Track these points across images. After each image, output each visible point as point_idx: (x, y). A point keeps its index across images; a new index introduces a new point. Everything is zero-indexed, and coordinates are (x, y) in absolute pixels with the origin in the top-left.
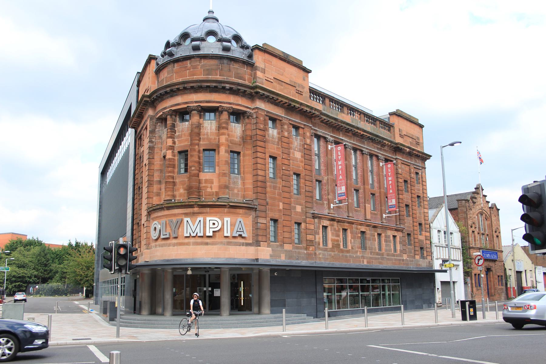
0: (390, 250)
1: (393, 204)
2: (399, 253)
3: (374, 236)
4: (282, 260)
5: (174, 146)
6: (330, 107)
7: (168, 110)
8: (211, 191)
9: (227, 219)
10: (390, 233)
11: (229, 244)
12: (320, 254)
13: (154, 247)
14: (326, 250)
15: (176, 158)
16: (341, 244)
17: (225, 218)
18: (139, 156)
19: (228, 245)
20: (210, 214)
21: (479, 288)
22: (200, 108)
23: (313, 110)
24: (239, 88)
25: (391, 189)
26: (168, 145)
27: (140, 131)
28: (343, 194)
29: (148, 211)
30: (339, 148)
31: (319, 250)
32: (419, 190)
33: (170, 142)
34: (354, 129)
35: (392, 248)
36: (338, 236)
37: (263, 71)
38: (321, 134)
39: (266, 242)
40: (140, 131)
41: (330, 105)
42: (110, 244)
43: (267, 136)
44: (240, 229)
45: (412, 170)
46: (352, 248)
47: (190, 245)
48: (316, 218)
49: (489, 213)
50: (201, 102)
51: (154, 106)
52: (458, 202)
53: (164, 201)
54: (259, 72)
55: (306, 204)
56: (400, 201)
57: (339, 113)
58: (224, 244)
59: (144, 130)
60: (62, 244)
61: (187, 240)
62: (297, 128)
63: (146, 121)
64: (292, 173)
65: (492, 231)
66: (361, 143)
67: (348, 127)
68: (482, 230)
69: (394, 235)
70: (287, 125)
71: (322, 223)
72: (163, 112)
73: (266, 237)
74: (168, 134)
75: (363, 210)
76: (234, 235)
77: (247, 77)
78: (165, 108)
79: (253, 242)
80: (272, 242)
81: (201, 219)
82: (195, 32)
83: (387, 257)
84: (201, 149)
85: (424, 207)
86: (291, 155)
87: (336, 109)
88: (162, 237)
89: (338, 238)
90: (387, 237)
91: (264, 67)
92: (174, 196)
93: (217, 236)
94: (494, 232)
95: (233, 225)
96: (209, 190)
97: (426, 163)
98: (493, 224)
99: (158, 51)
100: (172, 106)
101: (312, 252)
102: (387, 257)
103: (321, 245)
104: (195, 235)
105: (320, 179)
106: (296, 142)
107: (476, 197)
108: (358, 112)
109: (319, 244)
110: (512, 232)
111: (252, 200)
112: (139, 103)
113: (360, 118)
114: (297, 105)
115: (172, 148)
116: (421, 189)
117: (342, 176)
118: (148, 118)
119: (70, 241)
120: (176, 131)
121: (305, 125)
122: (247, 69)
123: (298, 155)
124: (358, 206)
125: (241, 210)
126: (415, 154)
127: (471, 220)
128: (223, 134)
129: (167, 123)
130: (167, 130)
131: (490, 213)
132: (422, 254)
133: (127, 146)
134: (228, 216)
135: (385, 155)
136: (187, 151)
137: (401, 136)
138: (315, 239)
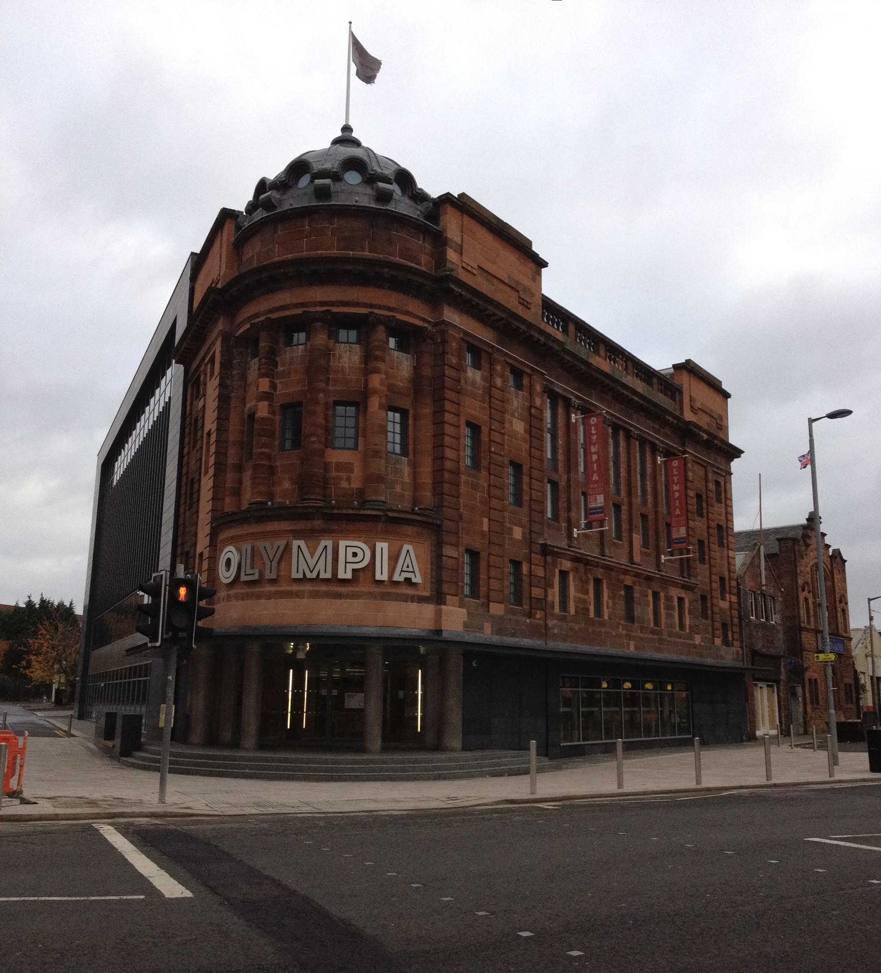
0: (672, 625)
1: (680, 536)
2: (688, 631)
3: (647, 596)
4: (487, 634)
5: (273, 394)
6: (576, 340)
7: (262, 318)
8: (347, 486)
9: (383, 547)
10: (675, 593)
11: (385, 596)
12: (554, 626)
13: (225, 601)
14: (563, 619)
15: (278, 418)
16: (592, 608)
17: (377, 543)
18: (194, 418)
19: (383, 599)
20: (347, 535)
21: (815, 706)
22: (329, 317)
23: (550, 341)
24: (410, 277)
25: (677, 507)
26: (261, 390)
27: (199, 366)
28: (598, 510)
29: (213, 525)
30: (593, 421)
31: (553, 619)
32: (720, 514)
33: (264, 385)
34: (619, 388)
35: (677, 620)
36: (586, 592)
37: (460, 250)
38: (560, 391)
39: (456, 596)
40: (199, 366)
41: (576, 336)
42: (154, 577)
43: (462, 382)
44: (408, 567)
45: (710, 475)
46: (610, 618)
47: (304, 598)
48: (549, 555)
49: (829, 567)
50: (332, 304)
51: (231, 315)
52: (780, 544)
53: (249, 504)
54: (451, 251)
55: (531, 525)
56: (690, 533)
57: (590, 353)
58: (375, 598)
59: (207, 364)
60: (13, 604)
61: (295, 588)
62: (518, 374)
63: (213, 343)
64: (506, 461)
65: (835, 601)
66: (625, 417)
67: (607, 382)
68: (806, 599)
69: (679, 595)
70: (501, 366)
71: (559, 566)
72: (251, 324)
73: (458, 586)
74: (260, 367)
75: (626, 545)
76: (397, 577)
77: (423, 258)
78: (256, 315)
79: (431, 594)
80: (466, 596)
81: (329, 543)
82: (319, 163)
83: (669, 639)
84: (331, 400)
85: (728, 546)
86: (507, 425)
87: (585, 346)
88: (243, 578)
89: (585, 597)
90: (669, 599)
91: (460, 243)
92: (271, 496)
93: (361, 579)
94: (837, 603)
95: (394, 559)
96: (344, 484)
97: (732, 464)
98: (837, 588)
99: (240, 201)
100: (271, 311)
101: (539, 622)
102: (669, 639)
103: (557, 609)
104: (314, 575)
105: (555, 477)
106: (516, 401)
107: (810, 535)
108: (623, 357)
109: (553, 607)
110: (869, 603)
111: (431, 508)
112: (192, 315)
113: (626, 369)
114: (523, 327)
115: (267, 396)
116: (724, 512)
117: (599, 476)
118: (216, 339)
119: (29, 597)
120: (277, 362)
121: (532, 369)
122: (424, 243)
123: (519, 427)
124: (619, 537)
125: (410, 527)
126: (717, 445)
127: (803, 578)
128: (377, 371)
129: (260, 345)
130: (260, 360)
131: (832, 565)
132: (725, 636)
133: (162, 404)
134: (384, 540)
135: (666, 444)
136: (300, 404)
137: (693, 410)
138: (546, 596)
